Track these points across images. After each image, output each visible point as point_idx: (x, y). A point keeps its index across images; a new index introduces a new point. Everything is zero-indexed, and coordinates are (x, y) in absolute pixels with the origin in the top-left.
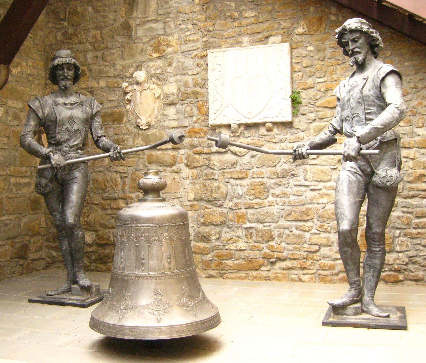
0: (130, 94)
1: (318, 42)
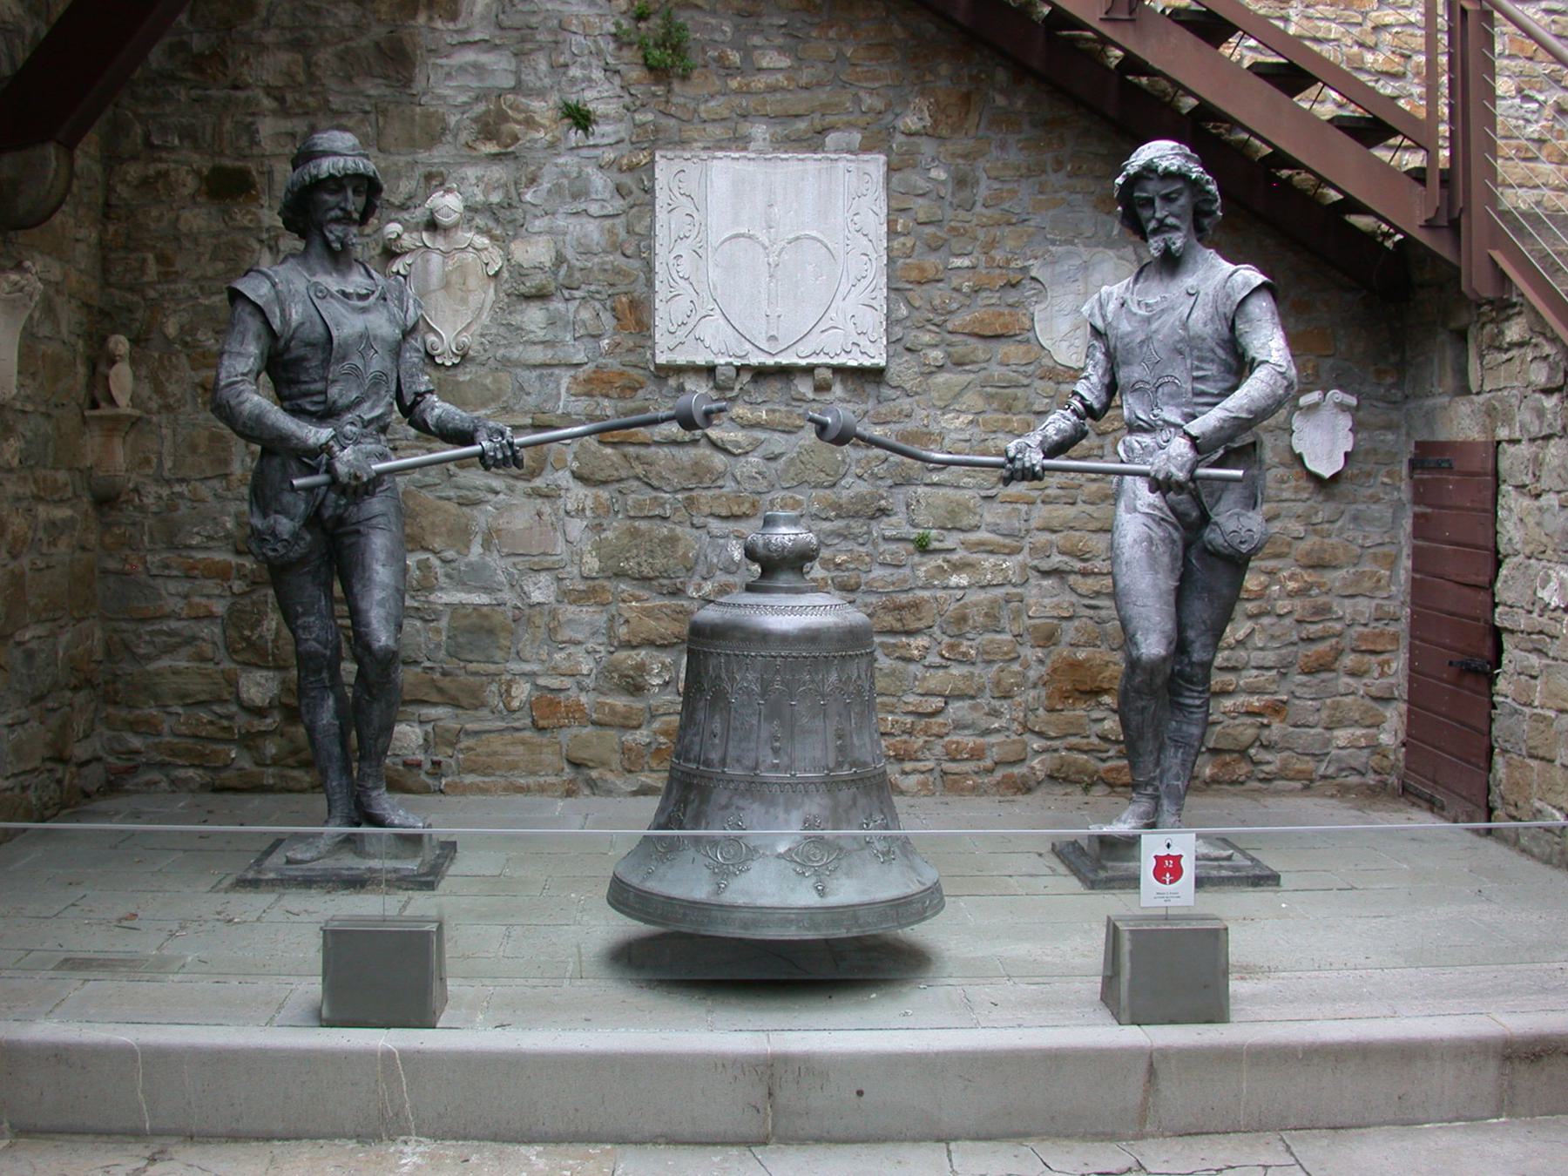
0: (408, 259)
1: (960, 161)
